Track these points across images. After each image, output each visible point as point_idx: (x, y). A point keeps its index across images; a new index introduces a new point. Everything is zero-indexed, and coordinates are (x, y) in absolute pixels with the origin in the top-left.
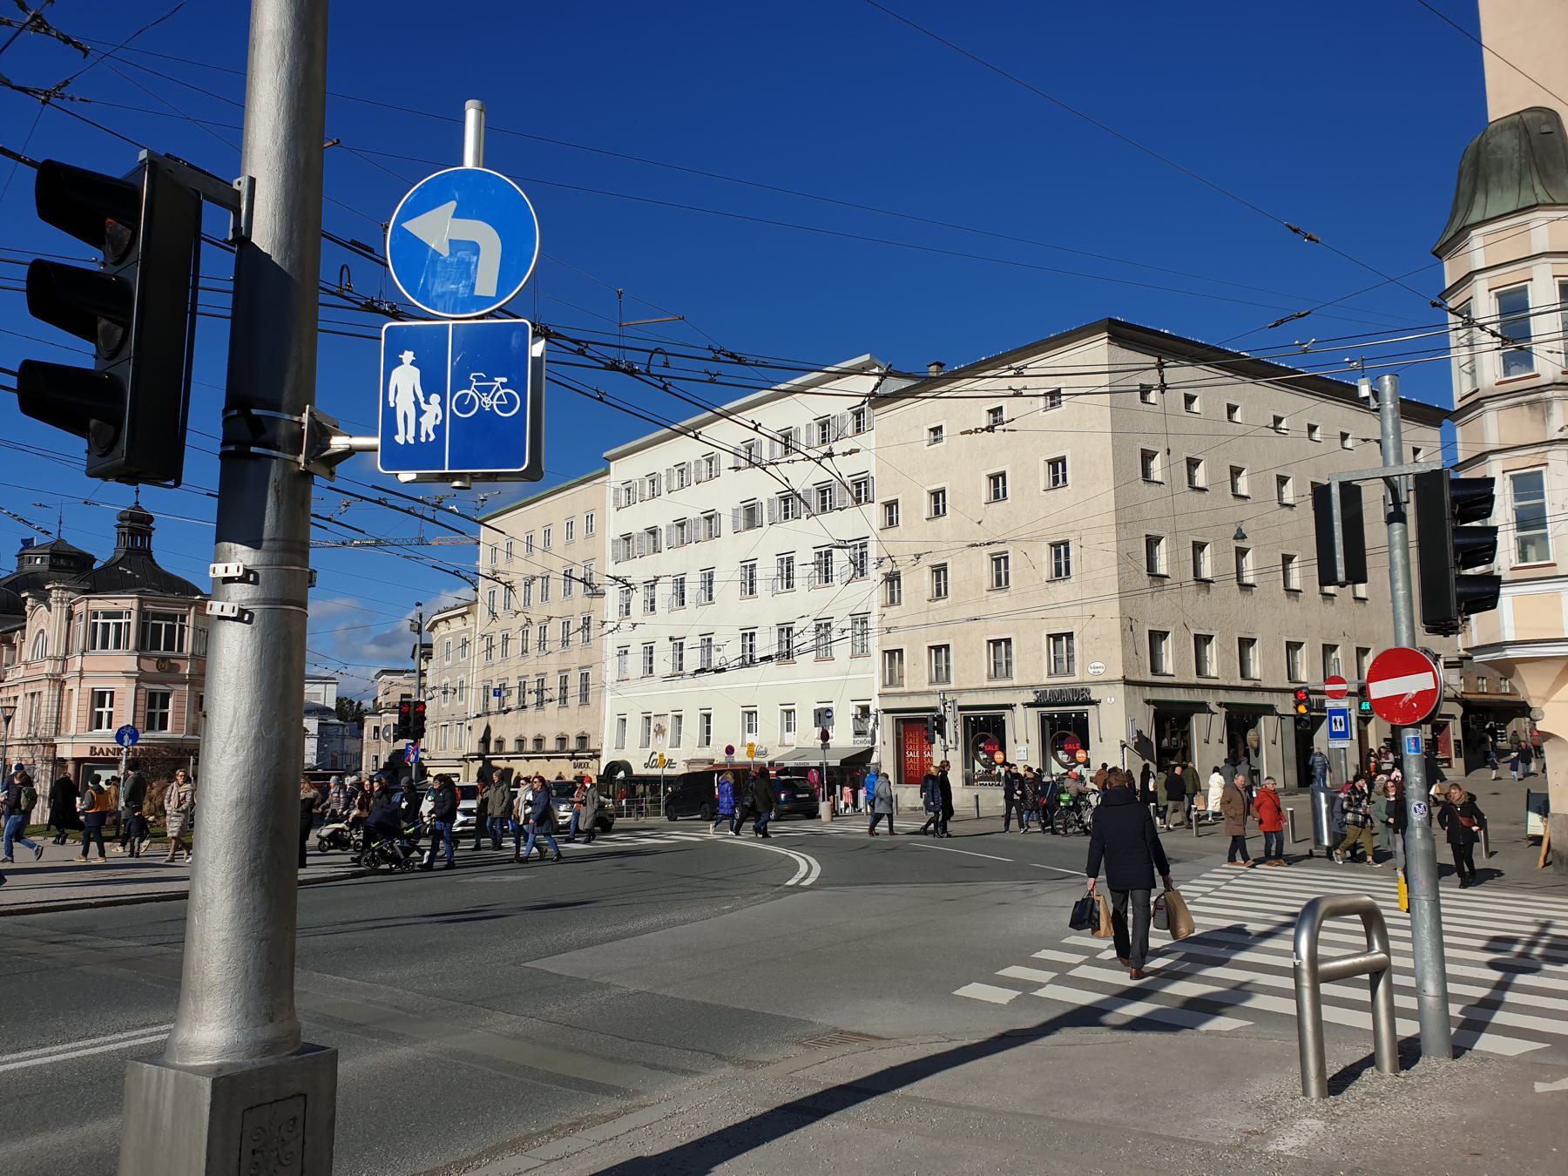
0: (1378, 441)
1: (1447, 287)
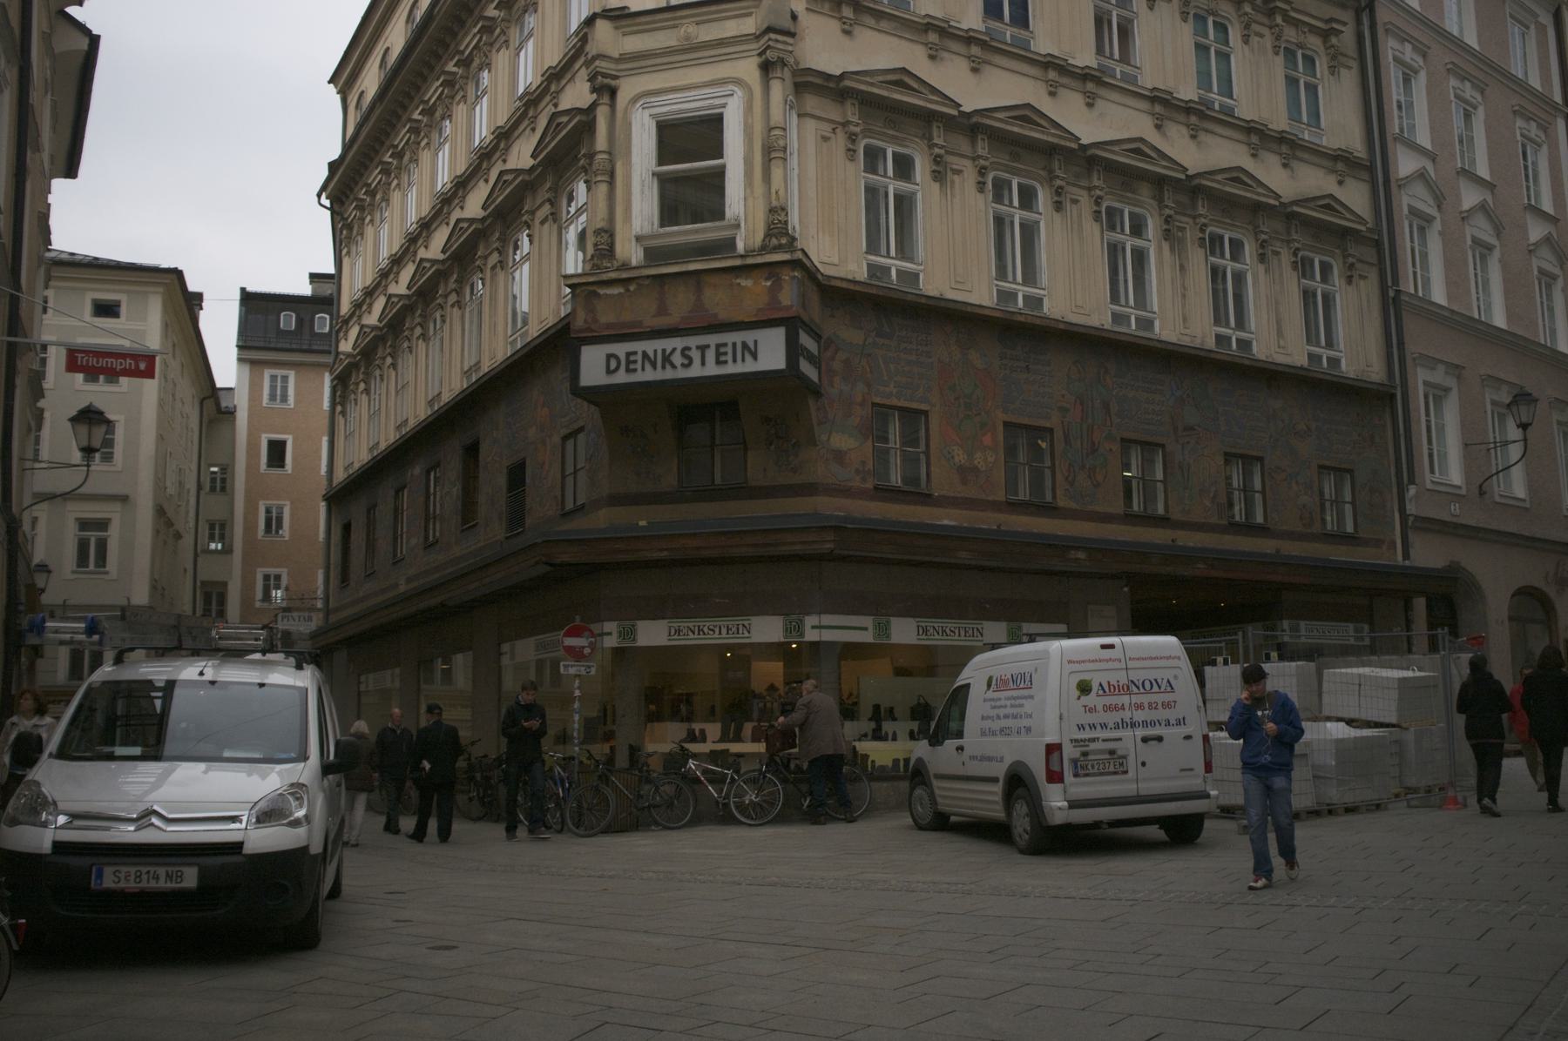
1: (25, 505)
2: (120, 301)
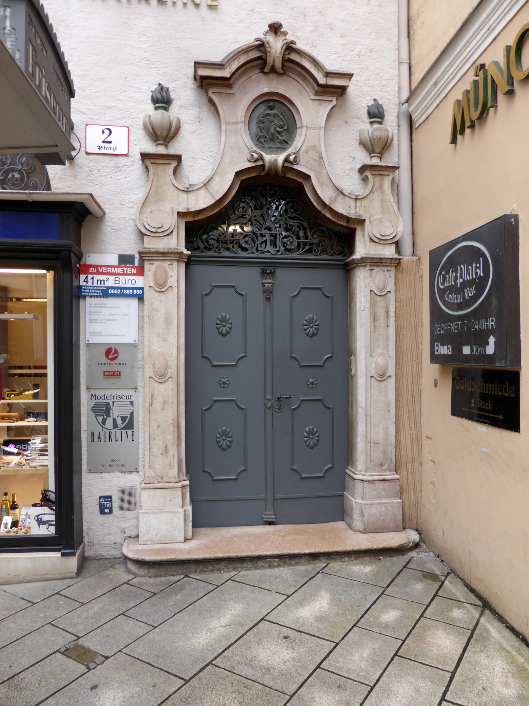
1: (416, 127)
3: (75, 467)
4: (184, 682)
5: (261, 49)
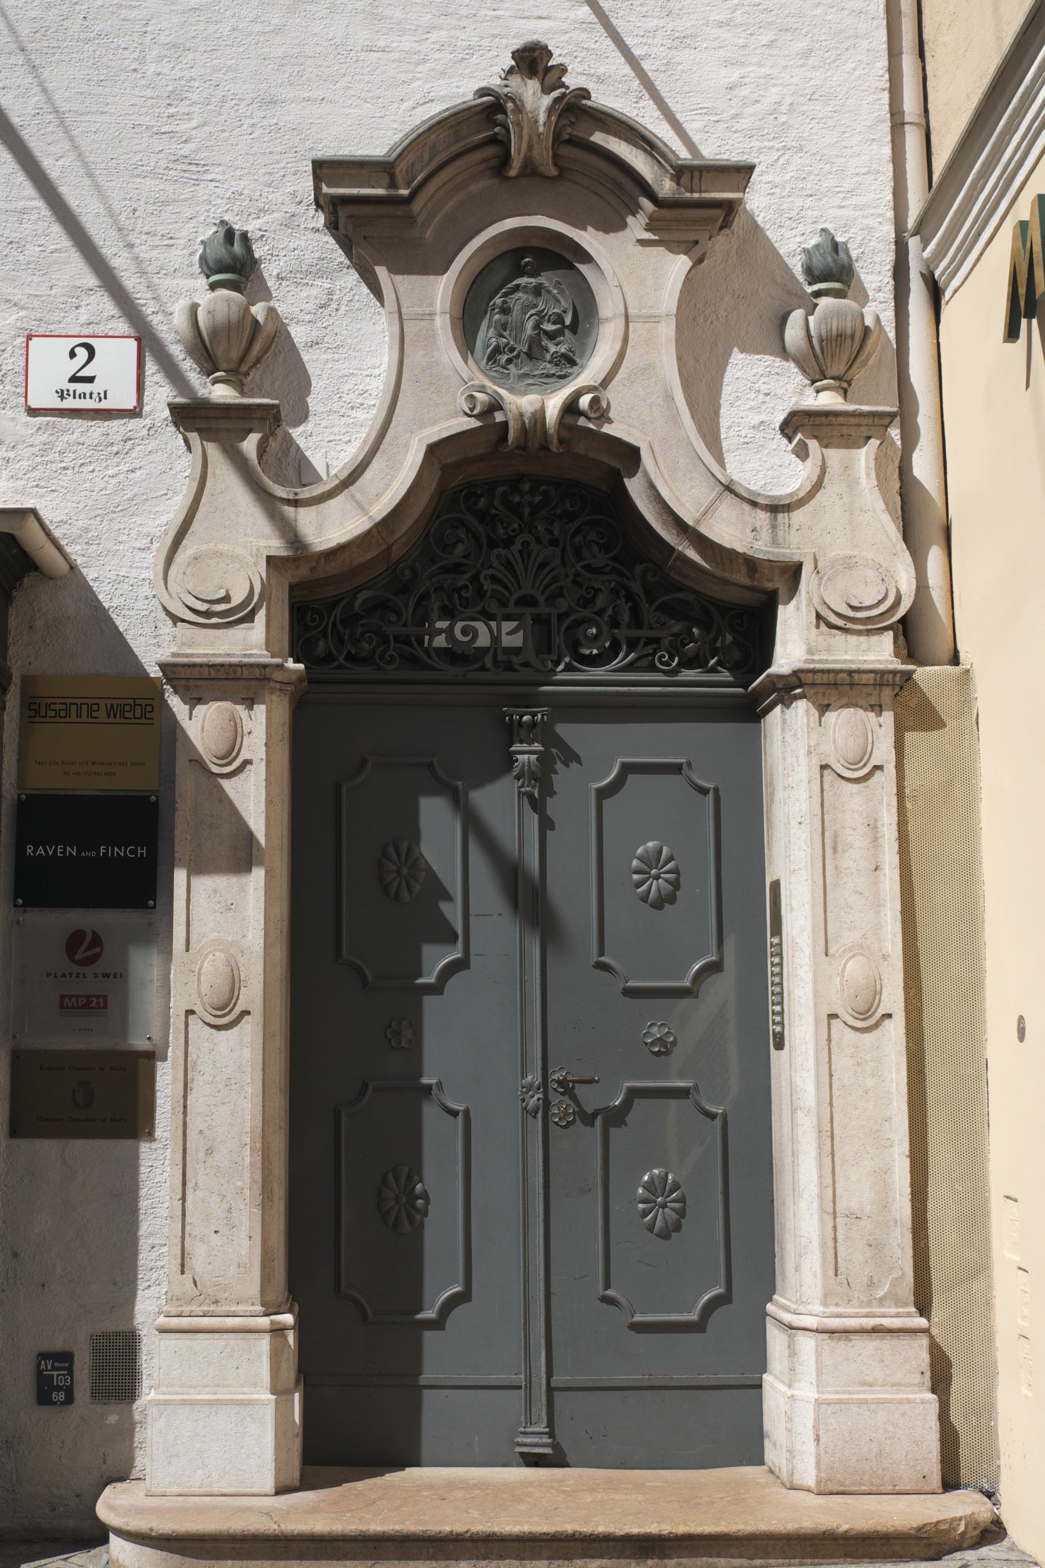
0: (29, 338)
2: (1018, 337)
3: (279, 1143)
4: (821, 621)
5: (205, 443)
